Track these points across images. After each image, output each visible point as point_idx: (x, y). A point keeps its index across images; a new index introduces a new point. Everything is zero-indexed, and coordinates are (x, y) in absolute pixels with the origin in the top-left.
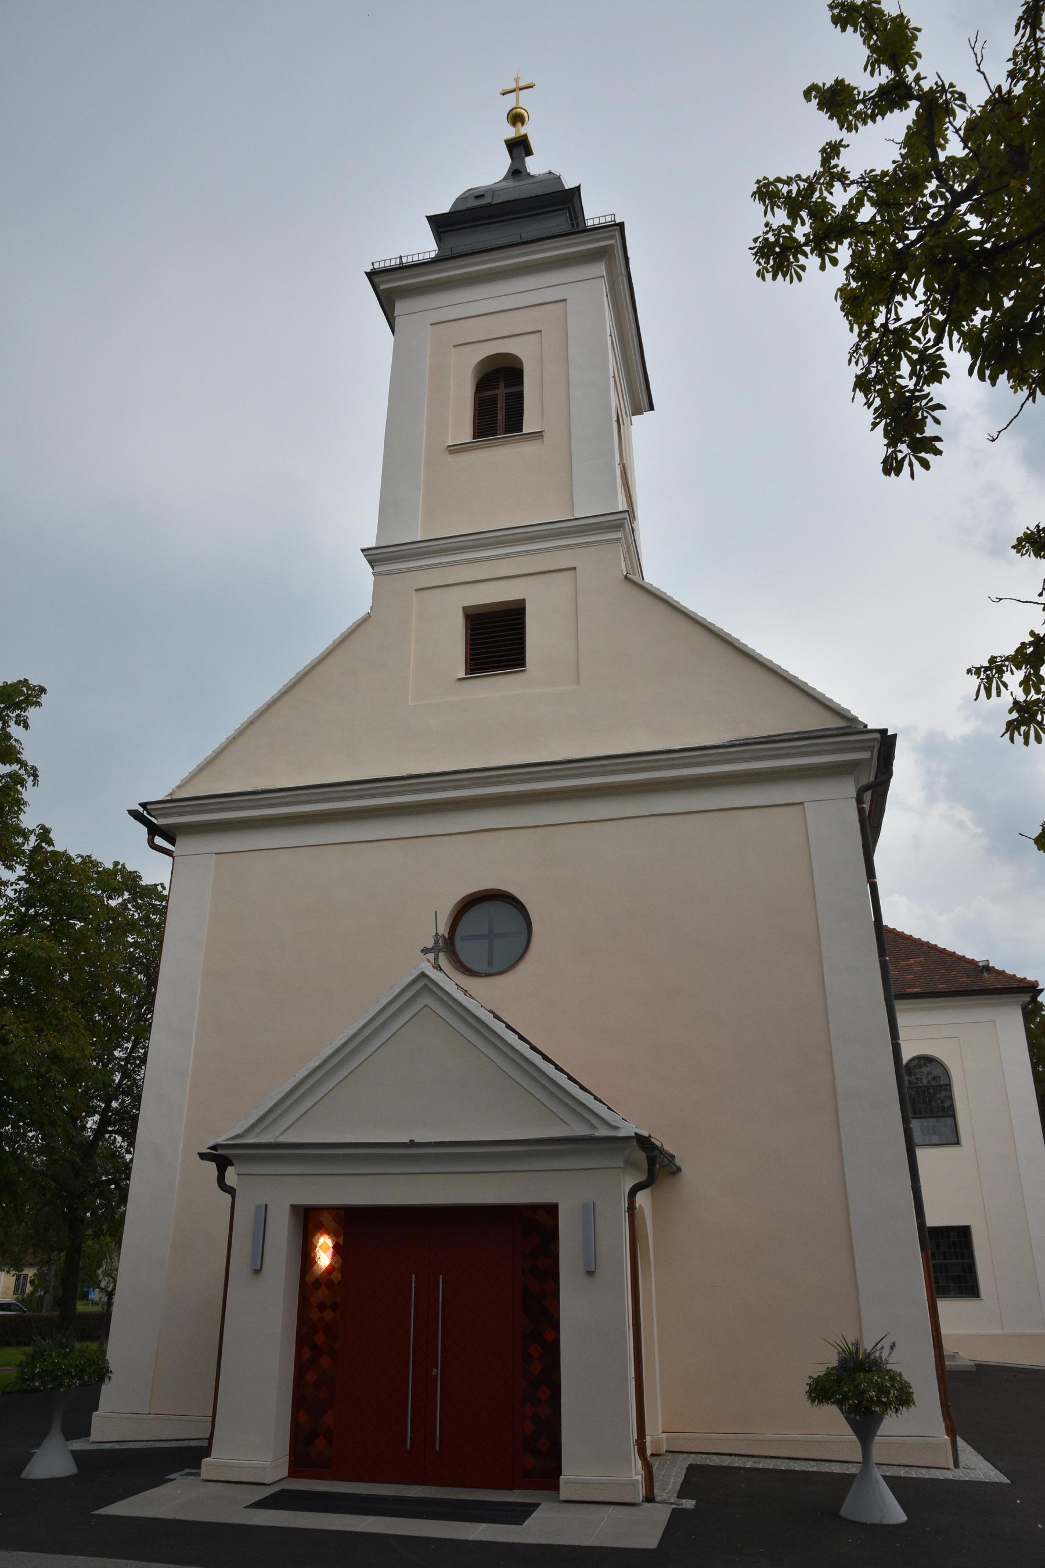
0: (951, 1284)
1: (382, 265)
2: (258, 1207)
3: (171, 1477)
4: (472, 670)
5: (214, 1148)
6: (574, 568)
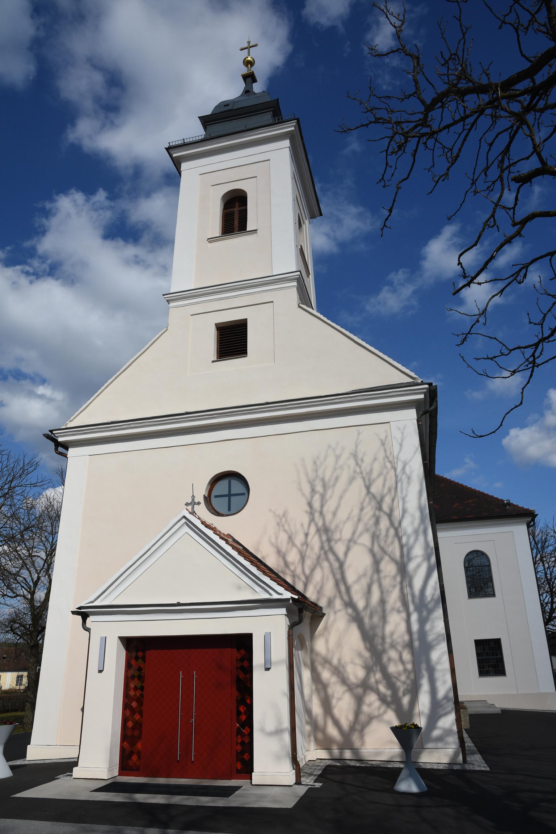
0: (491, 669)
1: (174, 144)
2: (102, 638)
3: (58, 777)
4: (220, 356)
5: (80, 608)
6: (272, 302)
